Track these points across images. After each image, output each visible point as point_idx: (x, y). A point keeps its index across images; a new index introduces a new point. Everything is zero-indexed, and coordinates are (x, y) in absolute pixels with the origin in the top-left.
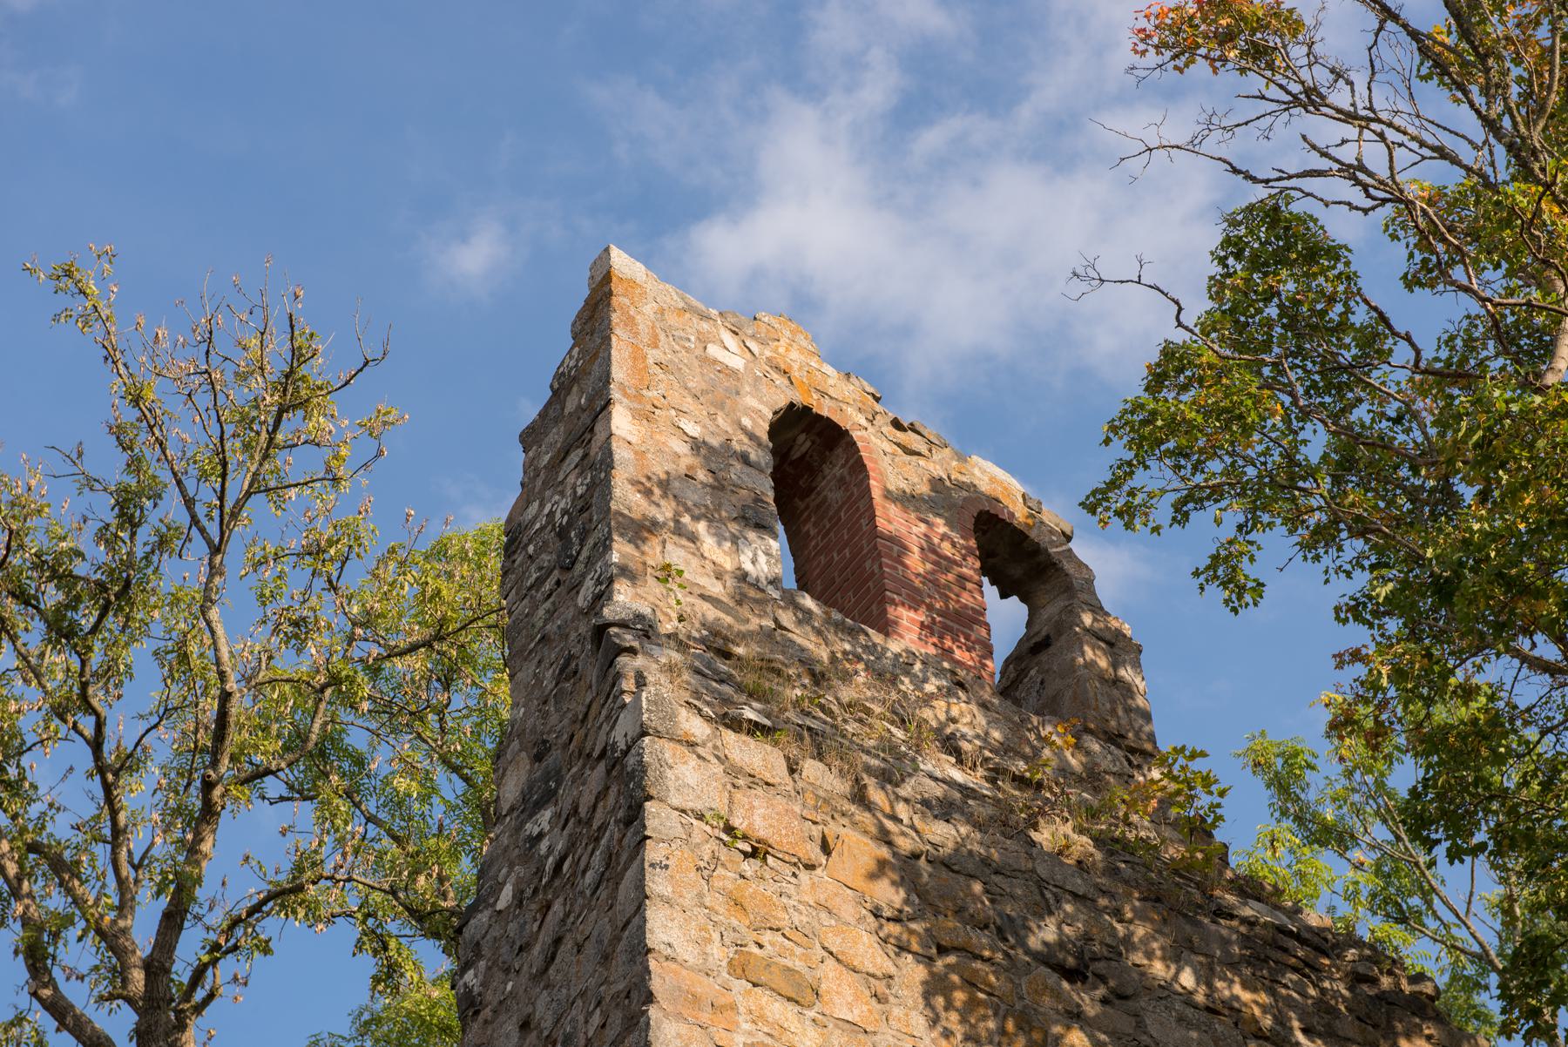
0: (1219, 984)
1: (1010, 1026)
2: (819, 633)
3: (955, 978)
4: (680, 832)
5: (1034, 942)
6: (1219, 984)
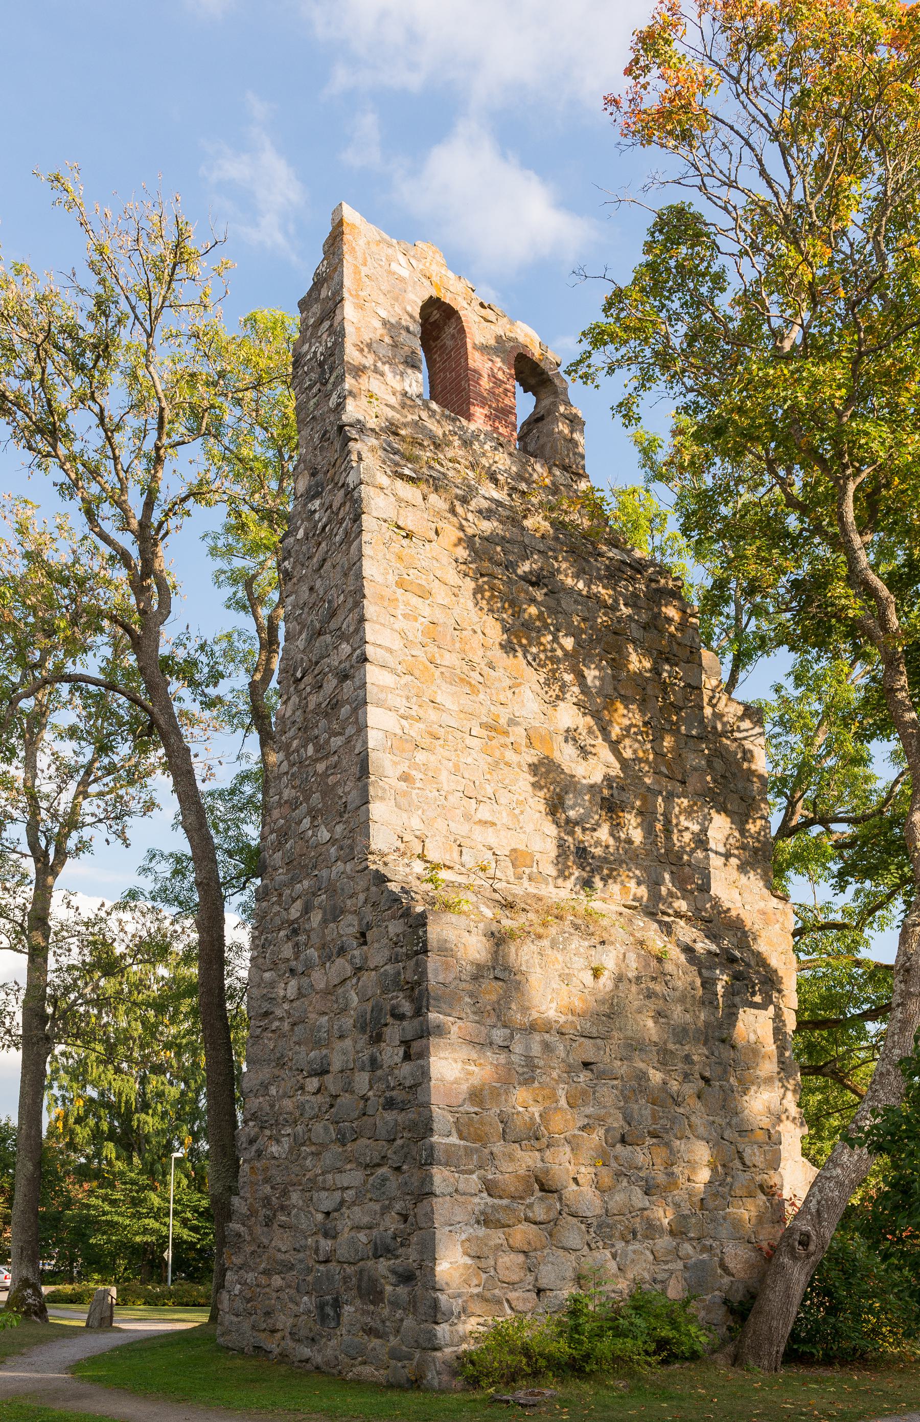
0: (593, 587)
1: (506, 605)
2: (439, 422)
3: (486, 587)
4: (376, 528)
5: (520, 572)
6: (593, 587)
